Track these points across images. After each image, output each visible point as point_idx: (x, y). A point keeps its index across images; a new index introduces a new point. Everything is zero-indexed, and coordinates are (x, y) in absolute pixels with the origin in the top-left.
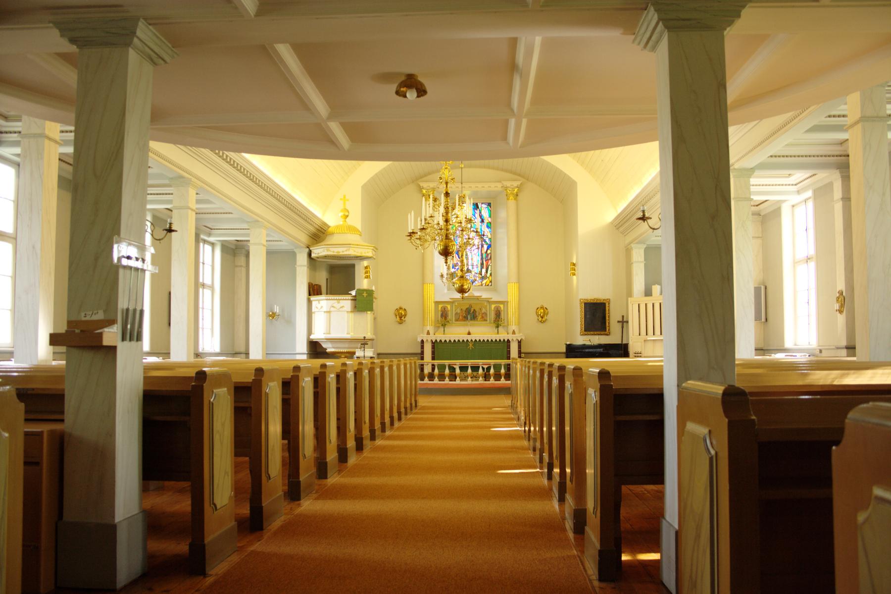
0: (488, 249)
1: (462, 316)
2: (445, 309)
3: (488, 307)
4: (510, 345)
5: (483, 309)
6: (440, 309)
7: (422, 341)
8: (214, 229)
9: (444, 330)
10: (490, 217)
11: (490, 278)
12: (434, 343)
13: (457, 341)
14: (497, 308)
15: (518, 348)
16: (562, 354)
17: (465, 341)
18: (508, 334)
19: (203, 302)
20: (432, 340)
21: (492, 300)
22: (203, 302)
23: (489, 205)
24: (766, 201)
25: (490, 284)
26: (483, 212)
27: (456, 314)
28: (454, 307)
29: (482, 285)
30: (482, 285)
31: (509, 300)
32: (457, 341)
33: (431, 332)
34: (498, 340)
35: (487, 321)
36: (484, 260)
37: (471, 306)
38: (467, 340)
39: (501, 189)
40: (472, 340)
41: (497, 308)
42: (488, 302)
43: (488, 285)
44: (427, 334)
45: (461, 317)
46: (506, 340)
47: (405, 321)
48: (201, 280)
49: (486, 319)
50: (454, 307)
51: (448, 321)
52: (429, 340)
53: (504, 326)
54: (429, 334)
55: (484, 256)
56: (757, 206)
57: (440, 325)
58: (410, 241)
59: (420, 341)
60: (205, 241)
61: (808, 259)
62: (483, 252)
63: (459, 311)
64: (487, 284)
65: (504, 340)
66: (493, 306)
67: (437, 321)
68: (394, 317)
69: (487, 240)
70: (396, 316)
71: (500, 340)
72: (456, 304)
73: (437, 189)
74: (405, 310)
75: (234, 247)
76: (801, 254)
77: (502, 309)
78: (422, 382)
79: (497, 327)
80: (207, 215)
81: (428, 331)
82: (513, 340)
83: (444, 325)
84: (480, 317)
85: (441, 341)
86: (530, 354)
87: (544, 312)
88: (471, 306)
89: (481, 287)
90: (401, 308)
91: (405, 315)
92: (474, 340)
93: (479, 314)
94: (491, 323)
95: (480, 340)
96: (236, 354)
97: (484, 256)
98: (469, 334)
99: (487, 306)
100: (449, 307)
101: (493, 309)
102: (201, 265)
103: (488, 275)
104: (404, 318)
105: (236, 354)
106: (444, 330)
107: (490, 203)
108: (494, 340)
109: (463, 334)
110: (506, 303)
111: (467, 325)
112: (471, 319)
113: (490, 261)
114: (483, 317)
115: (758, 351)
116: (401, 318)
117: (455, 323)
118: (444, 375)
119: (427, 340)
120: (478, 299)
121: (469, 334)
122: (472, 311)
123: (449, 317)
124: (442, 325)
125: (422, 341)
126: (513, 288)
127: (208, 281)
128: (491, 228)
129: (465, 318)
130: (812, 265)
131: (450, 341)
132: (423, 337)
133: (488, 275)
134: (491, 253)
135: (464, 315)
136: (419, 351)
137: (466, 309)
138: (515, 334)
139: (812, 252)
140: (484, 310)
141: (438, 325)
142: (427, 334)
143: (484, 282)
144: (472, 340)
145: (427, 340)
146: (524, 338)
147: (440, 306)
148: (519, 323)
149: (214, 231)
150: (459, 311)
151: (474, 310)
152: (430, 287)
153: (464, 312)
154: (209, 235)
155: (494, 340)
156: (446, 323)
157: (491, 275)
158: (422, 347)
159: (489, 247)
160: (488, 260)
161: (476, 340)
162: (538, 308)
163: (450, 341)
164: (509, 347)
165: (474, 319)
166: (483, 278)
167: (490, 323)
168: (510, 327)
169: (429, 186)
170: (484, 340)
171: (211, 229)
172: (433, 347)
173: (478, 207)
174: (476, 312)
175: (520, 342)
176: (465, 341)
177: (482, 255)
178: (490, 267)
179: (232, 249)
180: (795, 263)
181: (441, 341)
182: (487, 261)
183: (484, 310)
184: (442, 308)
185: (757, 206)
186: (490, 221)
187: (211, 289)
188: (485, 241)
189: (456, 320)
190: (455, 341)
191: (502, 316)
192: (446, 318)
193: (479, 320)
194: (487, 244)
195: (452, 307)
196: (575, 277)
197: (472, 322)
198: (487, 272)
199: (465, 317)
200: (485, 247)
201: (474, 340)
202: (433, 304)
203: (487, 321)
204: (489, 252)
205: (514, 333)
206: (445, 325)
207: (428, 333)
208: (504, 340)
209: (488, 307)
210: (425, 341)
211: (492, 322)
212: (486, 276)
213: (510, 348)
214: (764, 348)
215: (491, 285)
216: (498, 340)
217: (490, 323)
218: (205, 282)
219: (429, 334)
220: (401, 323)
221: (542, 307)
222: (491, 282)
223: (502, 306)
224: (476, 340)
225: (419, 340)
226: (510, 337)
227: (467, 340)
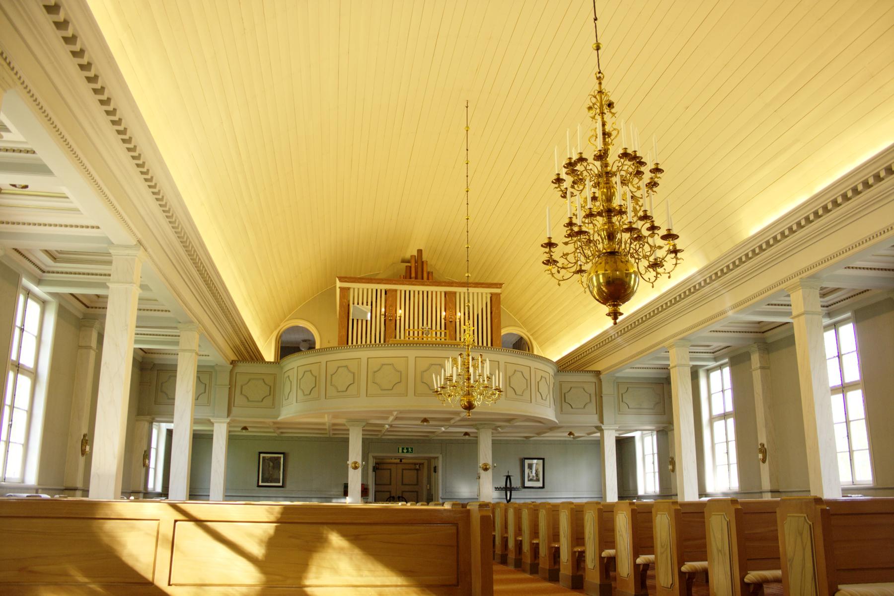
8: (49, 272)
19: (14, 395)
22: (20, 347)
24: (787, 323)
48: (14, 357)
56: (763, 332)
58: (559, 189)
60: (29, 294)
61: (725, 416)
75: (80, 316)
76: (718, 410)
80: (37, 227)
96: (66, 489)
102: (17, 332)
105: (66, 489)
115: (774, 494)
127: (27, 360)
130: (731, 422)
139: (730, 408)
149: (48, 274)
154: (39, 282)
171: (44, 272)
179: (78, 319)
180: (712, 420)
185: (763, 332)
187: (33, 376)
196: (403, 460)
214: (780, 490)
218: (21, 362)
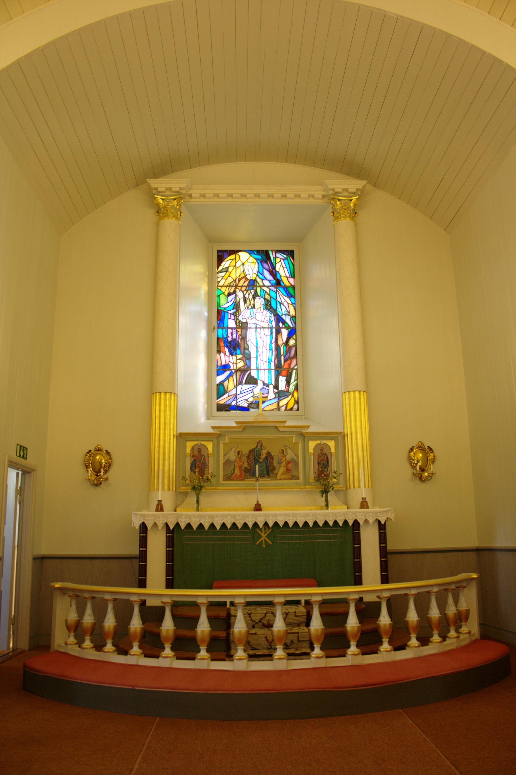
0: (289, 338)
1: (240, 467)
2: (199, 451)
3: (300, 446)
4: (359, 534)
5: (289, 451)
6: (188, 450)
7: (143, 527)
9: (198, 501)
10: (293, 276)
11: (296, 394)
12: (172, 532)
13: (229, 526)
14: (322, 450)
15: (380, 543)
16: (471, 553)
17: (250, 525)
18: (348, 508)
20: (167, 525)
21: (310, 430)
23: (290, 254)
25: (296, 407)
26: (278, 267)
27: (227, 463)
28: (221, 445)
29: (279, 408)
30: (279, 408)
31: (348, 431)
32: (229, 526)
33: (168, 505)
34: (331, 523)
35: (298, 478)
36: (282, 358)
37: (260, 444)
38: (256, 525)
39: (320, 202)
40: (266, 524)
41: (322, 450)
42: (302, 435)
43: (291, 409)
44: (157, 510)
45: (237, 471)
46: (351, 523)
47: (107, 479)
49: (294, 473)
50: (221, 445)
51: (208, 479)
52: (160, 525)
53: (337, 492)
54: (162, 510)
55: (283, 350)
57: (189, 489)
59: (137, 527)
62: (280, 342)
63: (232, 456)
64: (289, 407)
65: (346, 522)
66: (312, 445)
67: (181, 478)
68: (83, 469)
69: (288, 320)
70: (87, 467)
71: (336, 522)
72: (227, 440)
73: (187, 199)
74: (108, 453)
77: (333, 450)
78: (121, 659)
79: (325, 492)
81: (160, 502)
82: (366, 521)
83: (197, 489)
84: (282, 470)
85: (189, 525)
86: (399, 556)
87: (426, 459)
88: (260, 444)
89: (277, 413)
90: (99, 450)
91: (108, 467)
92: (271, 524)
93: (280, 463)
94: (310, 484)
95: (286, 523)
97: (283, 350)
98: (258, 508)
99: (296, 444)
100: (210, 446)
101: (311, 450)
103: (292, 388)
104: (106, 472)
106: (198, 501)
107: (292, 252)
108: (321, 524)
109: (243, 510)
110: (340, 439)
111: (253, 488)
112: (262, 476)
113: (294, 362)
114: (288, 471)
116: (97, 472)
117: (223, 485)
118: (193, 639)
119: (155, 524)
120: (277, 428)
121: (258, 508)
122: (263, 456)
123: (211, 469)
124: (194, 488)
125: (143, 527)
126: (358, 401)
128: (294, 297)
129: (249, 473)
131: (212, 526)
132: (144, 516)
133: (292, 388)
134: (295, 345)
135: (246, 465)
136: (135, 551)
137: (251, 452)
138: (367, 507)
140: (290, 455)
141: (183, 489)
142: (157, 510)
143: (283, 402)
144: (266, 524)
145: (155, 524)
146: (392, 516)
147: (190, 445)
148: (373, 484)
150: (232, 456)
151: (269, 454)
152: (165, 399)
153: (244, 459)
155: (321, 524)
156: (202, 484)
157: (297, 388)
158: (143, 542)
159: (292, 333)
160: (291, 359)
161: (276, 524)
162: (412, 449)
163: (212, 526)
164: (357, 539)
165: (268, 475)
166: (280, 395)
167: (306, 483)
168: (352, 492)
169: (170, 189)
170: (296, 523)
172: (170, 542)
173: (269, 258)
174: (272, 458)
175: (382, 527)
176: (250, 525)
177: (278, 348)
178: (294, 371)
181: (189, 525)
182: (289, 362)
183: (290, 455)
184: (193, 448)
186: (293, 284)
188: (284, 322)
189: (228, 478)
190: (224, 525)
191: (334, 467)
192: (202, 472)
193: (278, 477)
194: (287, 328)
195: (216, 448)
197: (266, 481)
198: (288, 383)
199: (246, 470)
200: (285, 333)
201: (271, 524)
202: (173, 442)
203: (298, 478)
204: (292, 342)
205: (364, 504)
206: (201, 487)
207: (160, 507)
208: (346, 522)
209: (300, 446)
210: (361, 522)
211: (312, 480)
212: (288, 391)
213: (359, 543)
215: (298, 409)
216: (331, 523)
217: (306, 483)
219: (162, 510)
220: (98, 485)
221: (421, 448)
222: (297, 402)
223: (331, 444)
224: (276, 524)
225: (137, 524)
226: (360, 515)
227: (256, 525)
